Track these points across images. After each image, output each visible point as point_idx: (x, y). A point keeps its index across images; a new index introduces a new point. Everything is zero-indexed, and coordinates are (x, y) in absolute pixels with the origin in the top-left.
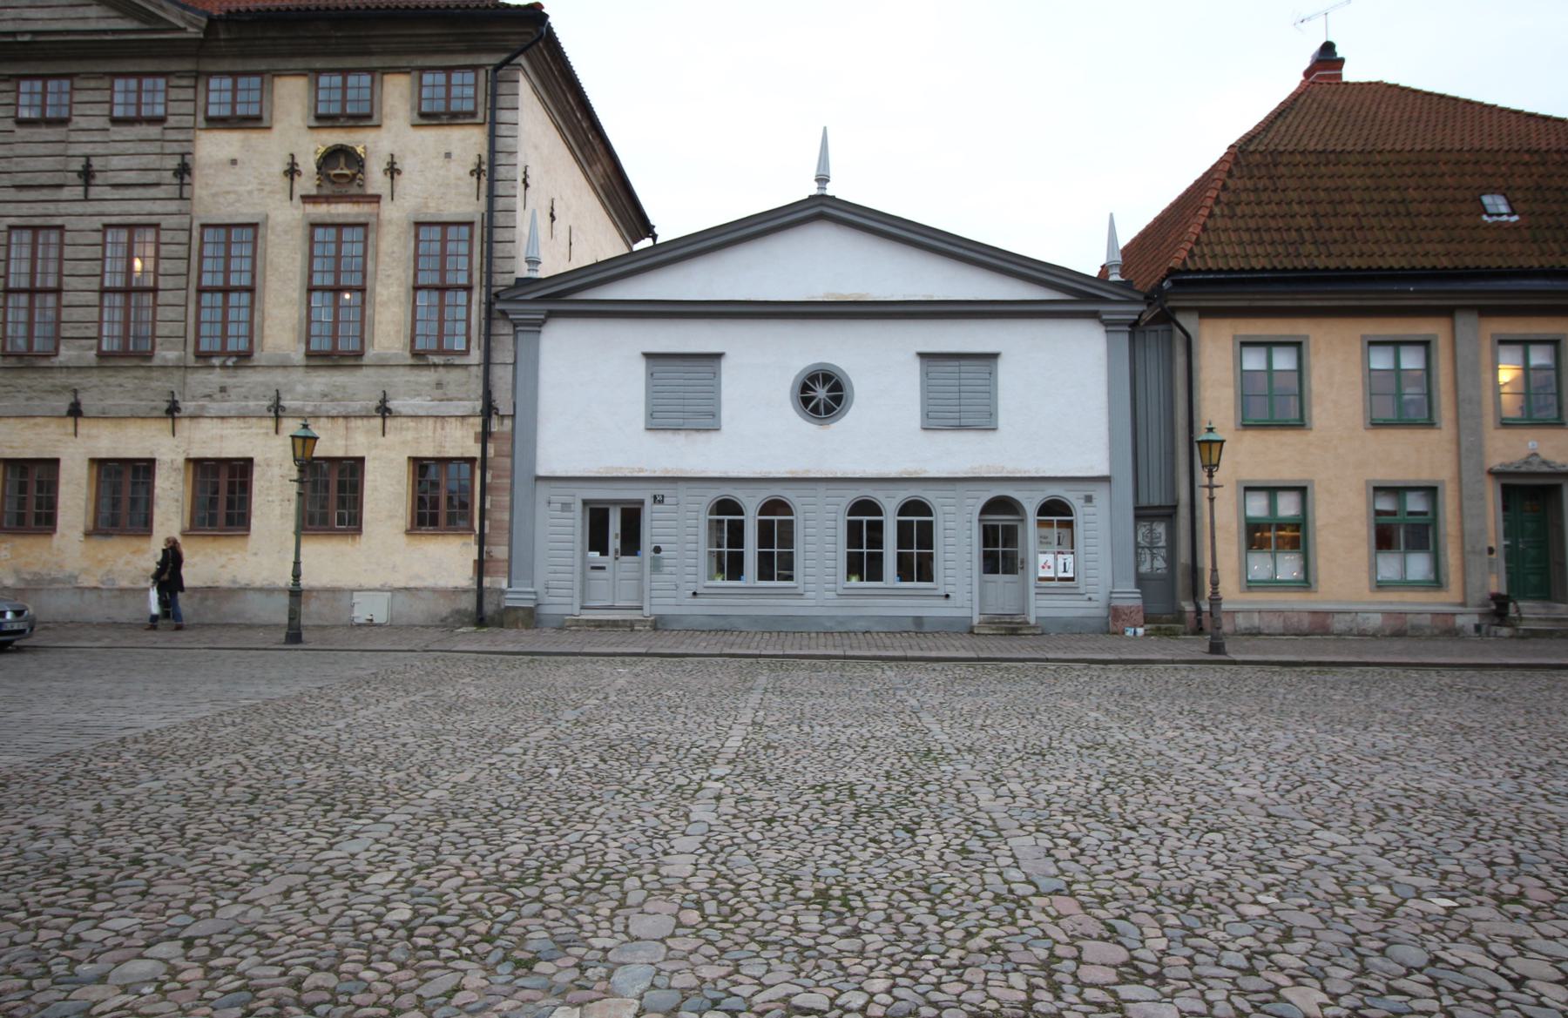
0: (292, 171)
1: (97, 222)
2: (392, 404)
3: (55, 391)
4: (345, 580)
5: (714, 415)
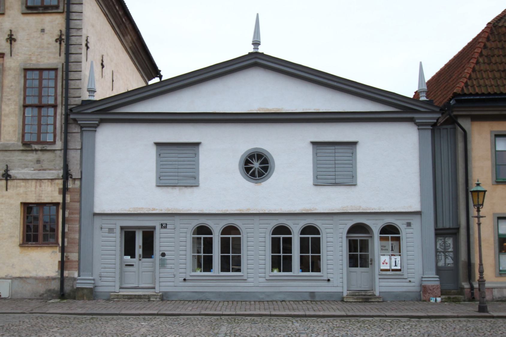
2: (12, 172)
5: (195, 178)
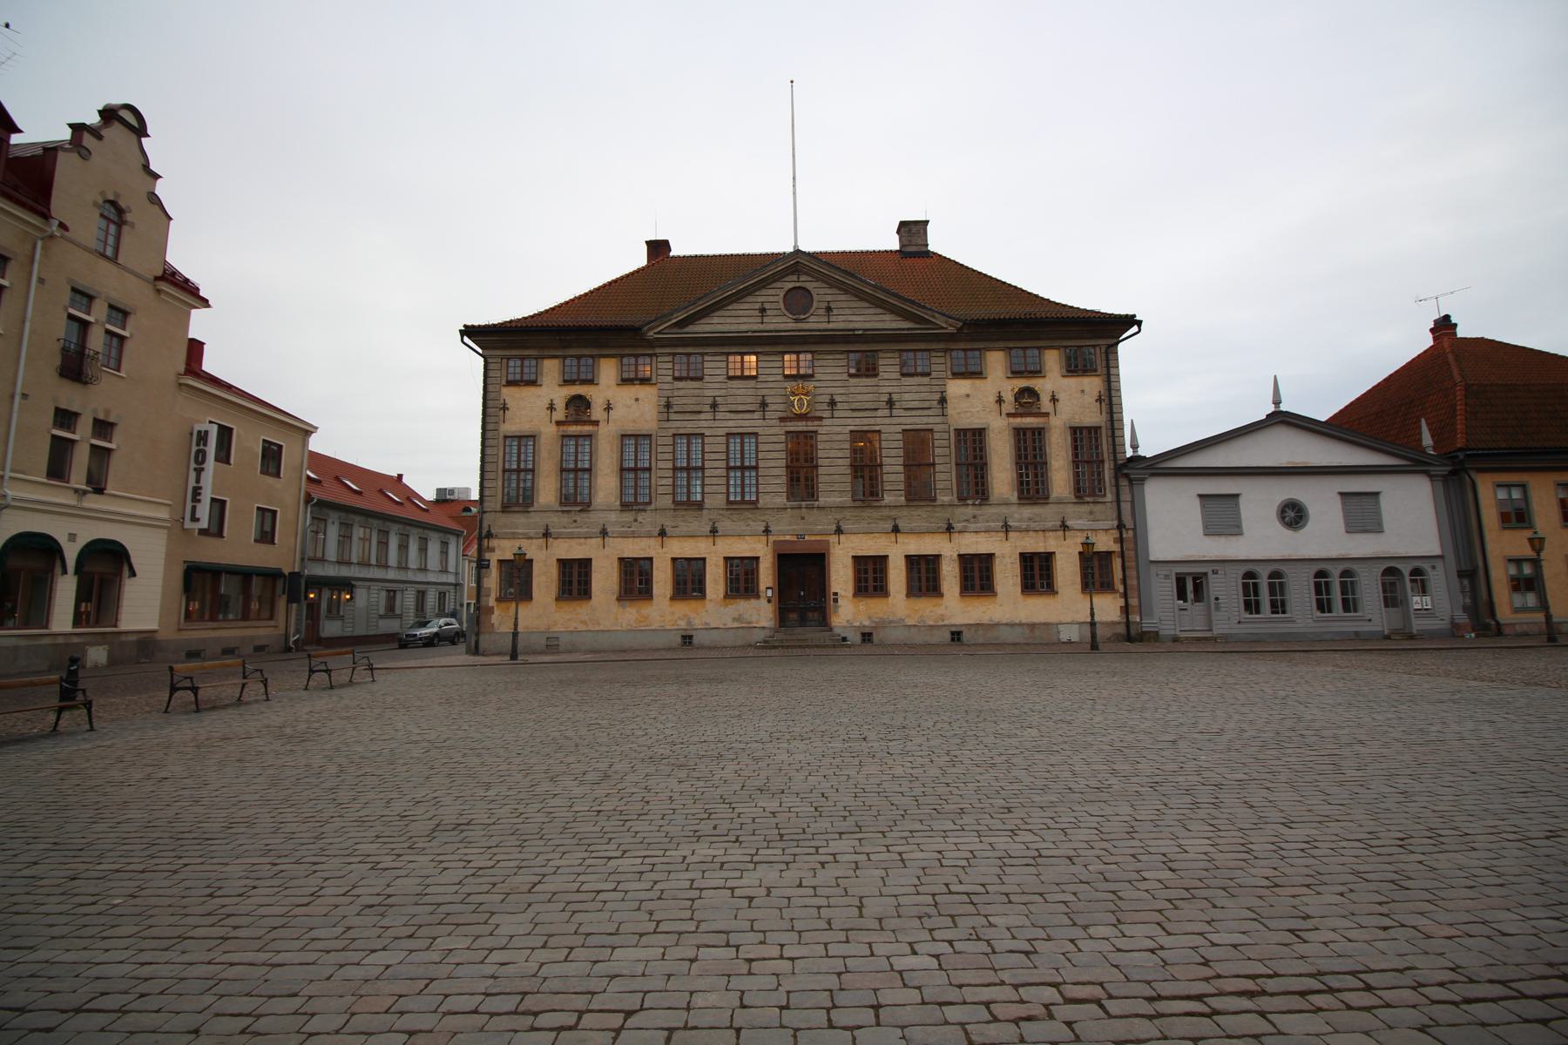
0: (1000, 401)
1: (723, 432)
2: (1069, 523)
3: (883, 519)
4: (1052, 619)
5: (1239, 526)
